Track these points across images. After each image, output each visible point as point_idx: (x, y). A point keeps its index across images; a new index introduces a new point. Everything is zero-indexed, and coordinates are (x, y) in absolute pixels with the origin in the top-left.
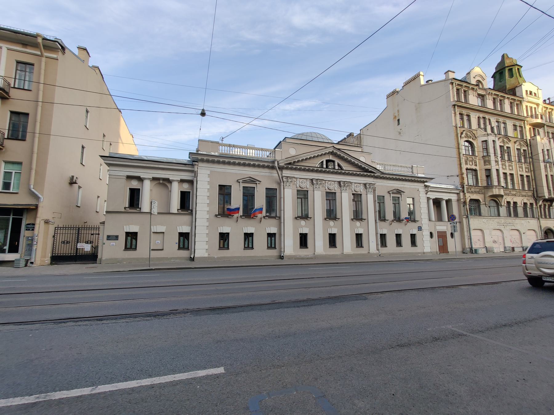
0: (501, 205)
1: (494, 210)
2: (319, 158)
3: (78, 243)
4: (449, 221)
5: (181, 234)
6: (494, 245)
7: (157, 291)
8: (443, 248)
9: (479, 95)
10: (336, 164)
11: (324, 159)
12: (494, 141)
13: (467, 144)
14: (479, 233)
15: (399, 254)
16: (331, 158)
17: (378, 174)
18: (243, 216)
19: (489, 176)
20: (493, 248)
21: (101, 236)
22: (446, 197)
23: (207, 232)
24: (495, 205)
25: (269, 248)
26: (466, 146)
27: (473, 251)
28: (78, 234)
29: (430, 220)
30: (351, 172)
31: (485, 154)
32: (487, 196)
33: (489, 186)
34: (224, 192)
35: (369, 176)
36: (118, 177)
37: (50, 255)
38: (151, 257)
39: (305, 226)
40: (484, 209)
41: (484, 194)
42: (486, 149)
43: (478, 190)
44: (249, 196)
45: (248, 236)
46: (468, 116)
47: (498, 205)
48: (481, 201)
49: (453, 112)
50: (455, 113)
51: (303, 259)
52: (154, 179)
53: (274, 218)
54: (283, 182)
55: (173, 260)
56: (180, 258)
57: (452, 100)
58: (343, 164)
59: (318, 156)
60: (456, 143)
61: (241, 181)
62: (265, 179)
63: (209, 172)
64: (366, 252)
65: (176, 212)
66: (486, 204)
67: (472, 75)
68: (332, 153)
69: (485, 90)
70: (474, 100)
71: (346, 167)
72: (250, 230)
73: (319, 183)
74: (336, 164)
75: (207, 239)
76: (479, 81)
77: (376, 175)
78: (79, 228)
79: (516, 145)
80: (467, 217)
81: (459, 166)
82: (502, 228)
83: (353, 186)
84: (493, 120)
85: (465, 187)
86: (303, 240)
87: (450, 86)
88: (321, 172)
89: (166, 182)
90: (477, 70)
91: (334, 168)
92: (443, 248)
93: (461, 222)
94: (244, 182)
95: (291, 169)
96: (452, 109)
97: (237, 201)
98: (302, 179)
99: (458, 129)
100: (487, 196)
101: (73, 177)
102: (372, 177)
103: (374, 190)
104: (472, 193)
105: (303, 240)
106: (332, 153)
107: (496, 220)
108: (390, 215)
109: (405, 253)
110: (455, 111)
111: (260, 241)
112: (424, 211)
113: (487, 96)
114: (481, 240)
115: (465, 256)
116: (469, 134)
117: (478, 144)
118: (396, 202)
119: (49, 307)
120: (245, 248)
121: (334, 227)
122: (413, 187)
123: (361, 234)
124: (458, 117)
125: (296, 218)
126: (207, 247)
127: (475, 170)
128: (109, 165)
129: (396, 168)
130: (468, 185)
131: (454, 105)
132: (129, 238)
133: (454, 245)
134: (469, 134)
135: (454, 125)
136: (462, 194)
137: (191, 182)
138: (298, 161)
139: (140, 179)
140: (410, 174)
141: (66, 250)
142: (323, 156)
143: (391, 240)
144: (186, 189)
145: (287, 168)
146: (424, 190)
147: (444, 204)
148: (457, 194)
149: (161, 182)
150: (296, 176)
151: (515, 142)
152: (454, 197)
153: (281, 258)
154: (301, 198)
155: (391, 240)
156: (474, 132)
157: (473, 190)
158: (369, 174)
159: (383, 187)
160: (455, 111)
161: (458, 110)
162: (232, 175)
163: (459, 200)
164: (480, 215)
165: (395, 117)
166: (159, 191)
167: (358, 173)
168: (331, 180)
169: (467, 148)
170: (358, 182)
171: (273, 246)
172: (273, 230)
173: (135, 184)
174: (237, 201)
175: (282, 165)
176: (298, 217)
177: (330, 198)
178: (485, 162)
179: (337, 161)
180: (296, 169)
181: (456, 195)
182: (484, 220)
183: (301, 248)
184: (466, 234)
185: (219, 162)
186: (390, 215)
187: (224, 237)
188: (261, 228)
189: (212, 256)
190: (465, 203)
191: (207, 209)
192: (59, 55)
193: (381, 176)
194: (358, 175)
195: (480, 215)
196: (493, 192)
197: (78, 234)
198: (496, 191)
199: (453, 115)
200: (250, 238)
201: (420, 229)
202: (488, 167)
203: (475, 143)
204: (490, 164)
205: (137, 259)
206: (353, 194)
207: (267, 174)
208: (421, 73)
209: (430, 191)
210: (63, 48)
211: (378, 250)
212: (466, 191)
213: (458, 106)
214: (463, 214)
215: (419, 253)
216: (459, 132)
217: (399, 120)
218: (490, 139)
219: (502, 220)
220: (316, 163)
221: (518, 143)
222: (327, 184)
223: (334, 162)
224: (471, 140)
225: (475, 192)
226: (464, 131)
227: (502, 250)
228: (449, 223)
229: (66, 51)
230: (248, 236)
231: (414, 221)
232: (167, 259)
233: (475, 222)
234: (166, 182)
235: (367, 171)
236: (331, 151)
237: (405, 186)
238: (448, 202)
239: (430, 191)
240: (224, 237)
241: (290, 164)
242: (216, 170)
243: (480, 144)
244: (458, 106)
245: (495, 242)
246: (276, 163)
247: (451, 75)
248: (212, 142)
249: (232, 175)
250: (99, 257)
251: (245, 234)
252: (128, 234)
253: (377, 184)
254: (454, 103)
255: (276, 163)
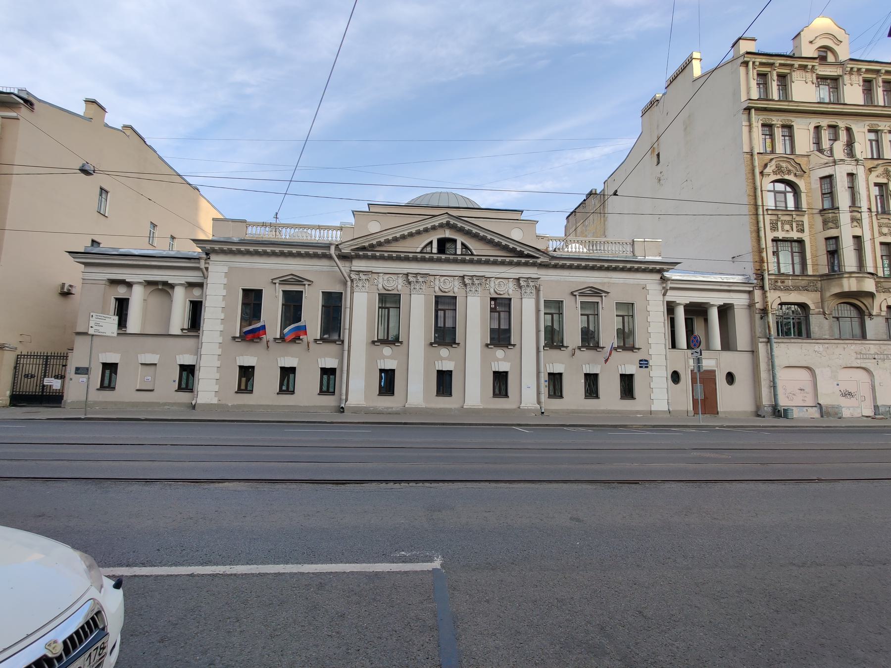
0: (870, 315)
1: (850, 324)
2: (425, 235)
3: (45, 376)
4: (689, 347)
5: (183, 368)
6: (844, 402)
7: (98, 450)
8: (706, 402)
9: (822, 79)
10: (459, 246)
11: (434, 238)
12: (851, 175)
13: (780, 187)
14: (805, 375)
15: (591, 412)
16: (448, 234)
17: (542, 259)
18: (582, 347)
19: (834, 254)
20: (839, 407)
21: (68, 367)
22: (716, 299)
23: (218, 364)
24: (854, 313)
25: (322, 392)
26: (776, 192)
27: (777, 412)
28: (46, 364)
29: (674, 346)
30: (492, 259)
31: (827, 205)
32: (828, 294)
33: (835, 272)
34: (252, 301)
35: (526, 264)
36: (95, 282)
37: (8, 393)
38: (89, 399)
39: (504, 359)
40: (817, 323)
41: (822, 291)
42: (830, 194)
43: (803, 283)
44: (293, 305)
45: (287, 373)
46: (789, 127)
47: (862, 314)
48: (812, 306)
49: (745, 123)
50: (750, 126)
51: (380, 413)
52: (149, 283)
53: (334, 342)
54: (352, 281)
55: (167, 407)
56: (325, 407)
57: (744, 97)
58: (473, 245)
59: (419, 233)
60: (752, 185)
61: (277, 281)
62: (318, 279)
63: (226, 269)
64: (514, 406)
65: (179, 332)
66: (824, 313)
67: (805, 37)
68: (448, 225)
69: (841, 64)
70: (804, 90)
71: (477, 248)
72: (289, 362)
73: (477, 282)
74: (459, 246)
75: (217, 376)
76: (826, 48)
77: (539, 261)
78: (47, 356)
79: (874, 174)
80: (769, 341)
81: (754, 235)
82: (869, 364)
83: (492, 284)
84: (861, 130)
85: (766, 277)
86: (388, 382)
87: (742, 70)
88: (423, 260)
89: (166, 288)
90: (822, 23)
91: (455, 254)
92: (706, 402)
93: (754, 352)
94: (582, 294)
95: (366, 257)
96: (745, 117)
97: (572, 327)
98: (388, 276)
99: (756, 157)
100: (828, 294)
101: (64, 284)
102: (534, 265)
103: (538, 290)
104: (787, 289)
105: (388, 382)
106: (448, 225)
107: (853, 347)
108: (572, 336)
109: (603, 412)
110: (749, 120)
111: (307, 382)
112: (653, 328)
113: (846, 78)
114: (809, 388)
115: (760, 422)
116: (784, 165)
117: (809, 186)
118: (591, 310)
119: (6, 462)
120: (281, 391)
121: (449, 359)
122: (631, 282)
123: (450, 373)
124: (757, 130)
125: (373, 342)
126: (216, 388)
127: (801, 242)
128: (86, 264)
129: (325, 233)
130: (780, 274)
131: (748, 109)
132: (185, 374)
133: (733, 401)
134: (784, 165)
135: (746, 149)
136: (758, 293)
137: (200, 285)
138: (388, 242)
139: (129, 285)
140: (628, 256)
141: (29, 387)
142: (432, 232)
143: (574, 387)
144: (197, 297)
145: (358, 257)
146: (660, 287)
147: (714, 314)
148: (749, 292)
149: (160, 287)
150: (487, 275)
151: (870, 170)
152: (739, 301)
153: (342, 410)
154: (552, 314)
155: (574, 387)
156: (803, 161)
157: (789, 283)
158: (523, 260)
159: (558, 284)
160: (749, 120)
161: (757, 120)
162: (262, 272)
163: (751, 306)
164: (809, 336)
165: (652, 148)
166: (156, 300)
167: (508, 259)
168: (446, 276)
169: (780, 197)
170: (502, 279)
171: (331, 390)
172: (330, 363)
173: (122, 292)
174: (572, 327)
175: (346, 250)
176: (379, 341)
177: (553, 311)
178: (825, 222)
179: (460, 239)
180: (374, 258)
181: (745, 296)
182: (819, 348)
183: (622, 398)
184: (764, 375)
185: (240, 253)
186: (572, 336)
187: (247, 373)
188: (309, 361)
189: (223, 402)
190: (764, 311)
191: (221, 328)
192: (24, 111)
193: (553, 262)
194: (503, 263)
195: (809, 336)
196: (842, 286)
197: (46, 364)
198: (850, 285)
199: (745, 130)
200: (291, 376)
201: (644, 364)
202: (833, 233)
203: (801, 183)
204: (836, 224)
205: (115, 403)
206: (492, 299)
207: (325, 269)
208: (696, 55)
209: (672, 288)
210: (29, 103)
211: (539, 402)
212: (767, 287)
213: (757, 109)
214: (758, 334)
215: (638, 412)
216: (756, 163)
217: (658, 155)
218: (841, 173)
219: (871, 348)
220: (416, 245)
221: (880, 170)
222: (437, 282)
223: (454, 241)
224: (791, 178)
225: (797, 288)
226: (772, 160)
227: (869, 412)
228: (690, 352)
229: (37, 105)
230: (287, 373)
231: (632, 349)
232: (158, 404)
233: (788, 352)
234: (166, 288)
235: (521, 254)
236: (444, 221)
237: (612, 281)
238: (725, 311)
239: (672, 288)
240: (556, 379)
241: (363, 248)
242: (237, 265)
243: (816, 185)
244: (757, 109)
245: (848, 394)
246: (333, 248)
247: (745, 46)
248: (233, 221)
249: (262, 272)
250: (65, 398)
251: (282, 369)
252: (106, 366)
253: (543, 278)
254: (745, 105)
255: (333, 248)
